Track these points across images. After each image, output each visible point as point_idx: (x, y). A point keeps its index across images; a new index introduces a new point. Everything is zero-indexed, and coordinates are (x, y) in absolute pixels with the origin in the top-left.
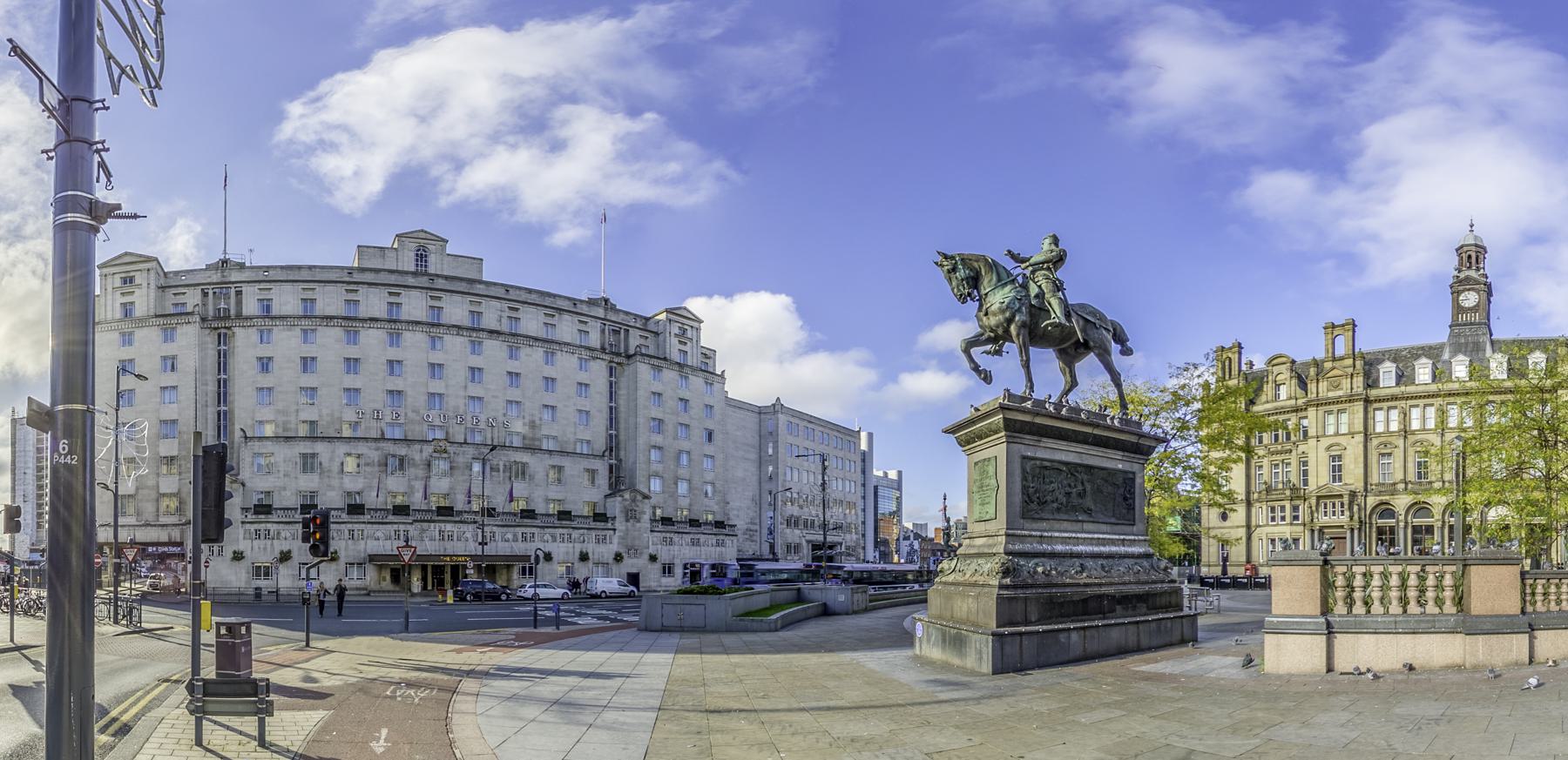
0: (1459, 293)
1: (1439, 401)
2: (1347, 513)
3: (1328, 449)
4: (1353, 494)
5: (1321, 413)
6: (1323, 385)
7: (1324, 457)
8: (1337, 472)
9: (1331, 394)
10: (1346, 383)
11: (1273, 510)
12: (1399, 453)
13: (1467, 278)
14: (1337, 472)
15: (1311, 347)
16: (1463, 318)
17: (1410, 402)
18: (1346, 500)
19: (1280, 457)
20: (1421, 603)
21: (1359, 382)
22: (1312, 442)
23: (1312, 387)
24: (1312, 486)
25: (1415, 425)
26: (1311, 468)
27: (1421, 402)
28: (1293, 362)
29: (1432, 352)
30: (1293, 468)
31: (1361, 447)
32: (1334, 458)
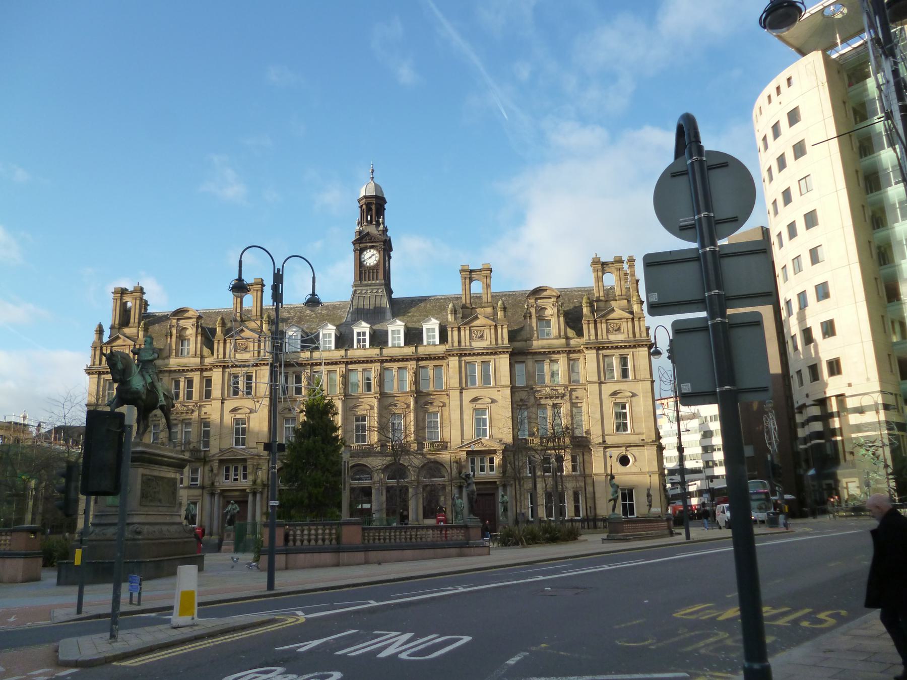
23: (218, 347)
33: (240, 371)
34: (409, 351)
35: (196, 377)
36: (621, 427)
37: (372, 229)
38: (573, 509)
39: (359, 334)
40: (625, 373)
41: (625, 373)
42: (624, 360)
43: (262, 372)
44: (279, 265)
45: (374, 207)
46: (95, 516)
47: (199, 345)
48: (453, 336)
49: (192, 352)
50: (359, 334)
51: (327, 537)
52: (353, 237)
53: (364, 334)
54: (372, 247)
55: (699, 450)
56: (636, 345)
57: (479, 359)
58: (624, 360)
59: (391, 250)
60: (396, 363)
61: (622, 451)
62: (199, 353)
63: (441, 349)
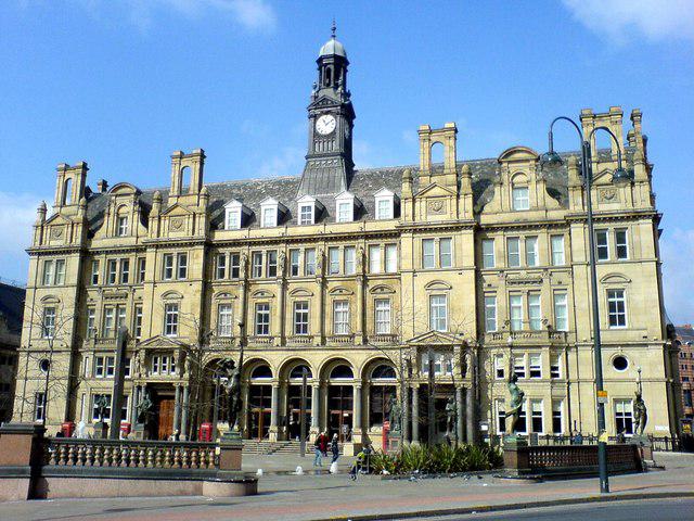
0: (316, 117)
1: (361, 243)
2: (177, 370)
3: (165, 295)
4: (185, 349)
5: (418, 242)
6: (421, 205)
7: (160, 303)
8: (171, 323)
9: (172, 235)
10: (450, 204)
11: (100, 361)
12: (239, 304)
13: (325, 99)
14: (171, 323)
15: (156, 177)
16: (319, 149)
17: (331, 244)
18: (176, 354)
19: (115, 302)
20: (162, 461)
21: (467, 203)
22: (148, 288)
23: (153, 224)
24: (144, 337)
25: (376, 268)
26: (145, 316)
27: (382, 242)
28: (138, 193)
29: (285, 189)
30: (127, 316)
31: (199, 296)
32: (170, 307)
33: (174, 251)
34: (355, 227)
35: (133, 259)
36: (617, 319)
37: (329, 93)
38: (551, 422)
39: (304, 208)
40: (621, 252)
41: (621, 252)
42: (620, 237)
43: (196, 252)
44: (586, 139)
45: (335, 69)
46: (173, 398)
47: (135, 223)
48: (406, 208)
49: (129, 232)
50: (304, 208)
51: (211, 459)
52: (310, 101)
53: (309, 207)
54: (327, 113)
55: (549, 377)
56: (636, 216)
57: (611, 226)
58: (620, 237)
59: (353, 117)
60: (614, 224)
61: (618, 352)
62: (134, 231)
63: (392, 225)
